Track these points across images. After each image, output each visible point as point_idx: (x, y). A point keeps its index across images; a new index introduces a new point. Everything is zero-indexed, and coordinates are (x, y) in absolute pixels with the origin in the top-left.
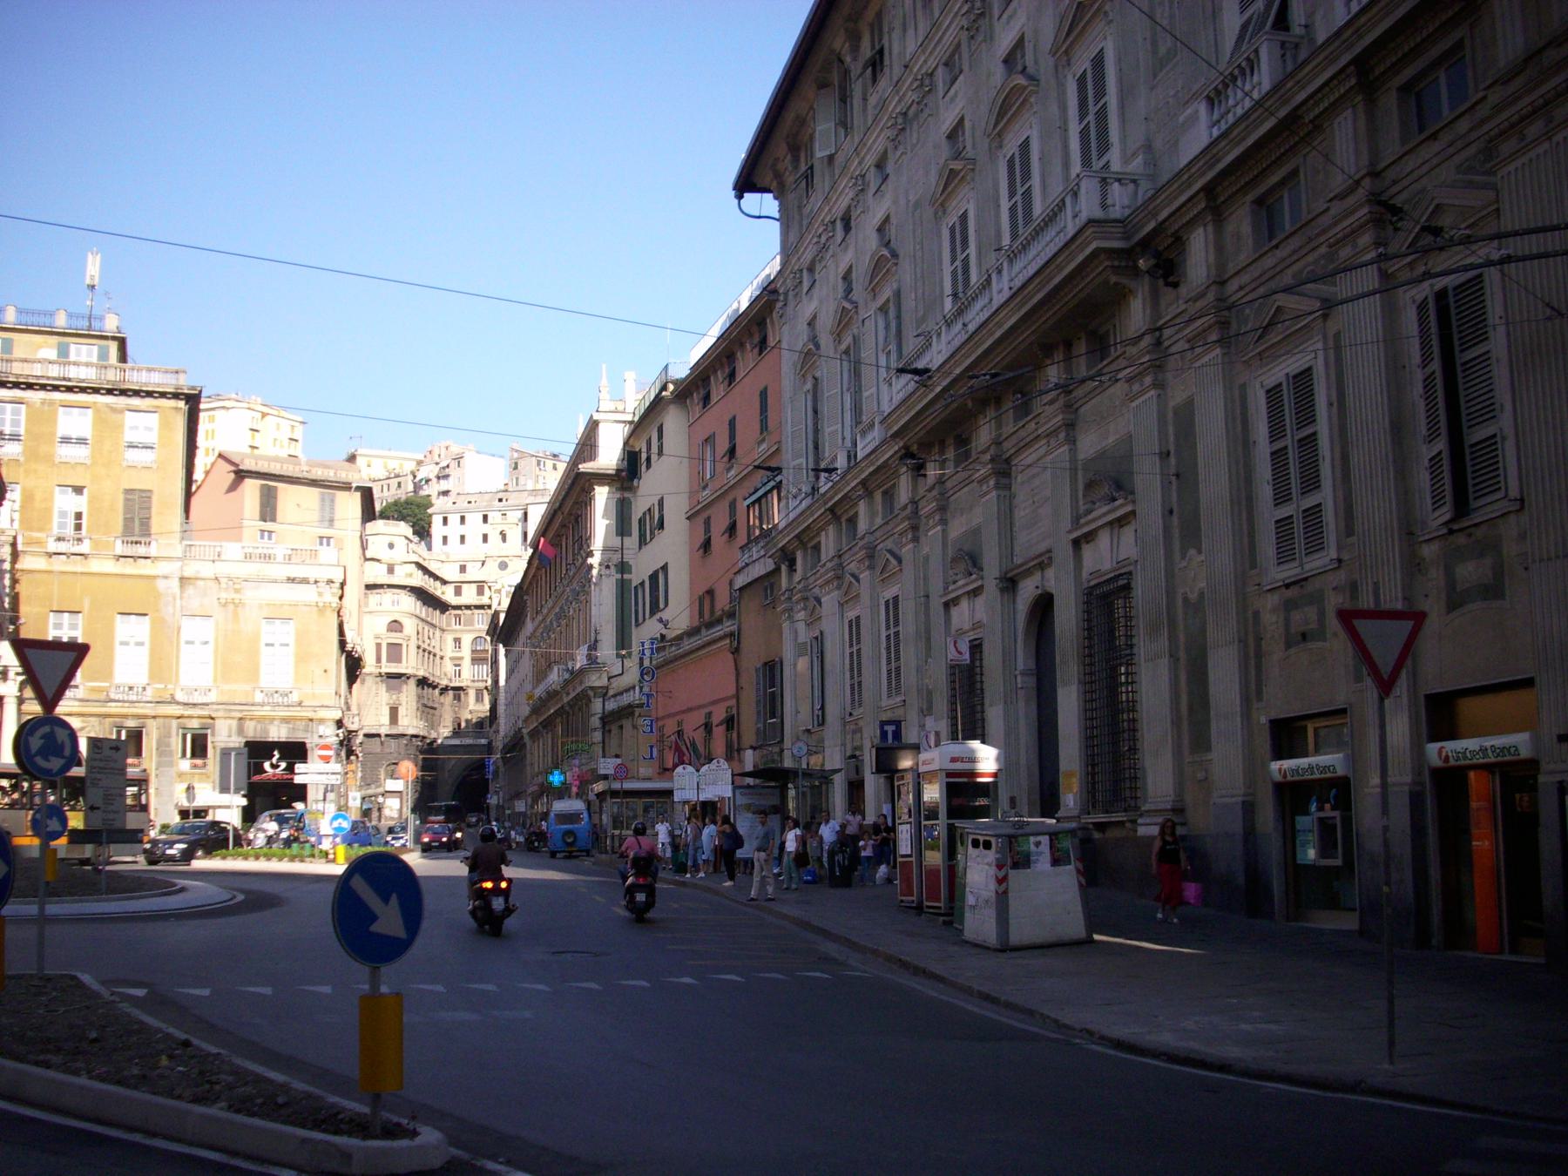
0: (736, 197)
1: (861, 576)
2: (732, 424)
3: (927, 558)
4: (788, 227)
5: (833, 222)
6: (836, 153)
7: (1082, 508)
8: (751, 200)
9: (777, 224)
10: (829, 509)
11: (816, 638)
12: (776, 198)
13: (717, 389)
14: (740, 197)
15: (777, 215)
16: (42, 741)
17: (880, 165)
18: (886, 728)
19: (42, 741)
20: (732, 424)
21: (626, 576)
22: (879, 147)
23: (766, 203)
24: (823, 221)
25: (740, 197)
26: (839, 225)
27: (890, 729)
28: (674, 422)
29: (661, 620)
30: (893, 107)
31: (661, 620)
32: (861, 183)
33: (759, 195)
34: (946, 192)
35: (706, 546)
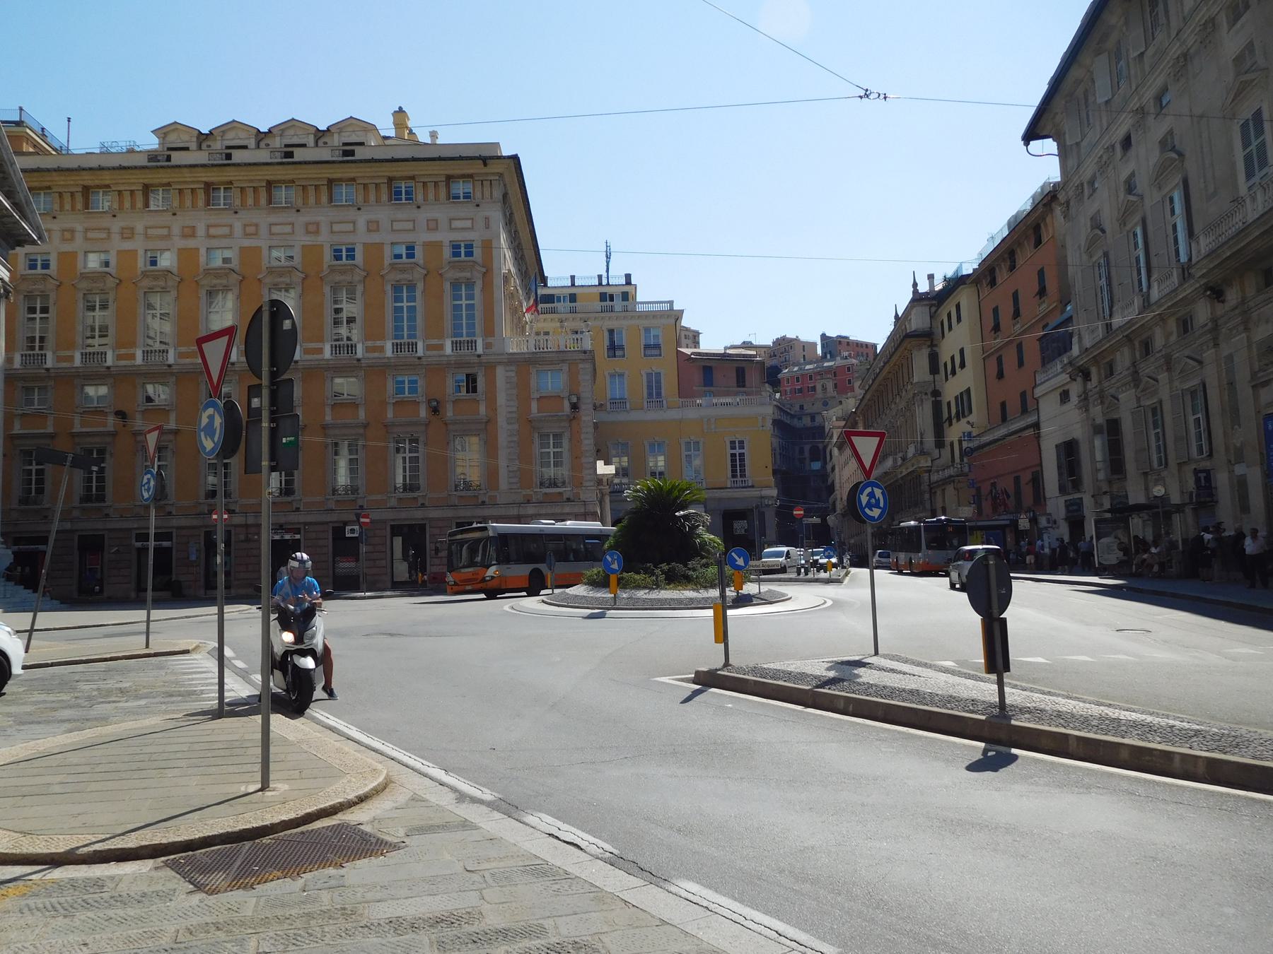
0: (1024, 144)
1: (1120, 396)
2: (1015, 296)
3: (1230, 358)
4: (1066, 157)
5: (1113, 146)
6: (1113, 96)
7: (1256, 367)
8: (1035, 145)
9: (1057, 158)
10: (1127, 336)
11: (1193, 393)
12: (1054, 140)
13: (1002, 275)
14: (1027, 144)
15: (1056, 153)
16: (3, 692)
17: (1159, 98)
18: (1200, 475)
19: (3, 692)
20: (1015, 296)
21: (938, 399)
22: (1159, 82)
23: (1050, 145)
24: (1103, 146)
25: (1027, 144)
26: (1118, 148)
27: (1202, 475)
28: (965, 298)
29: (968, 422)
30: (1175, 51)
31: (968, 422)
32: (1141, 112)
33: (1041, 141)
34: (1236, 102)
35: (1000, 375)
